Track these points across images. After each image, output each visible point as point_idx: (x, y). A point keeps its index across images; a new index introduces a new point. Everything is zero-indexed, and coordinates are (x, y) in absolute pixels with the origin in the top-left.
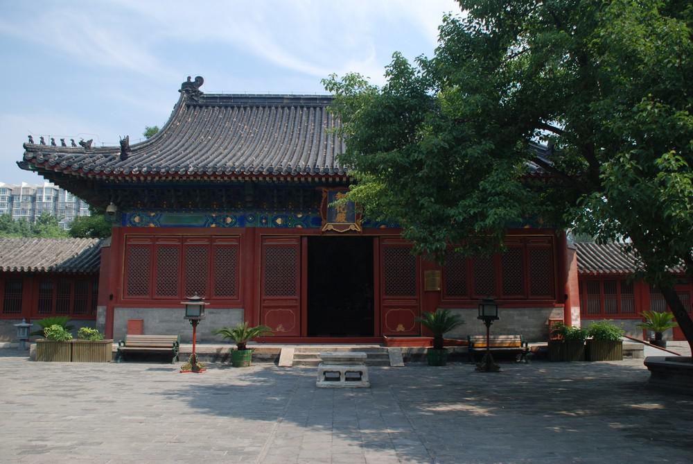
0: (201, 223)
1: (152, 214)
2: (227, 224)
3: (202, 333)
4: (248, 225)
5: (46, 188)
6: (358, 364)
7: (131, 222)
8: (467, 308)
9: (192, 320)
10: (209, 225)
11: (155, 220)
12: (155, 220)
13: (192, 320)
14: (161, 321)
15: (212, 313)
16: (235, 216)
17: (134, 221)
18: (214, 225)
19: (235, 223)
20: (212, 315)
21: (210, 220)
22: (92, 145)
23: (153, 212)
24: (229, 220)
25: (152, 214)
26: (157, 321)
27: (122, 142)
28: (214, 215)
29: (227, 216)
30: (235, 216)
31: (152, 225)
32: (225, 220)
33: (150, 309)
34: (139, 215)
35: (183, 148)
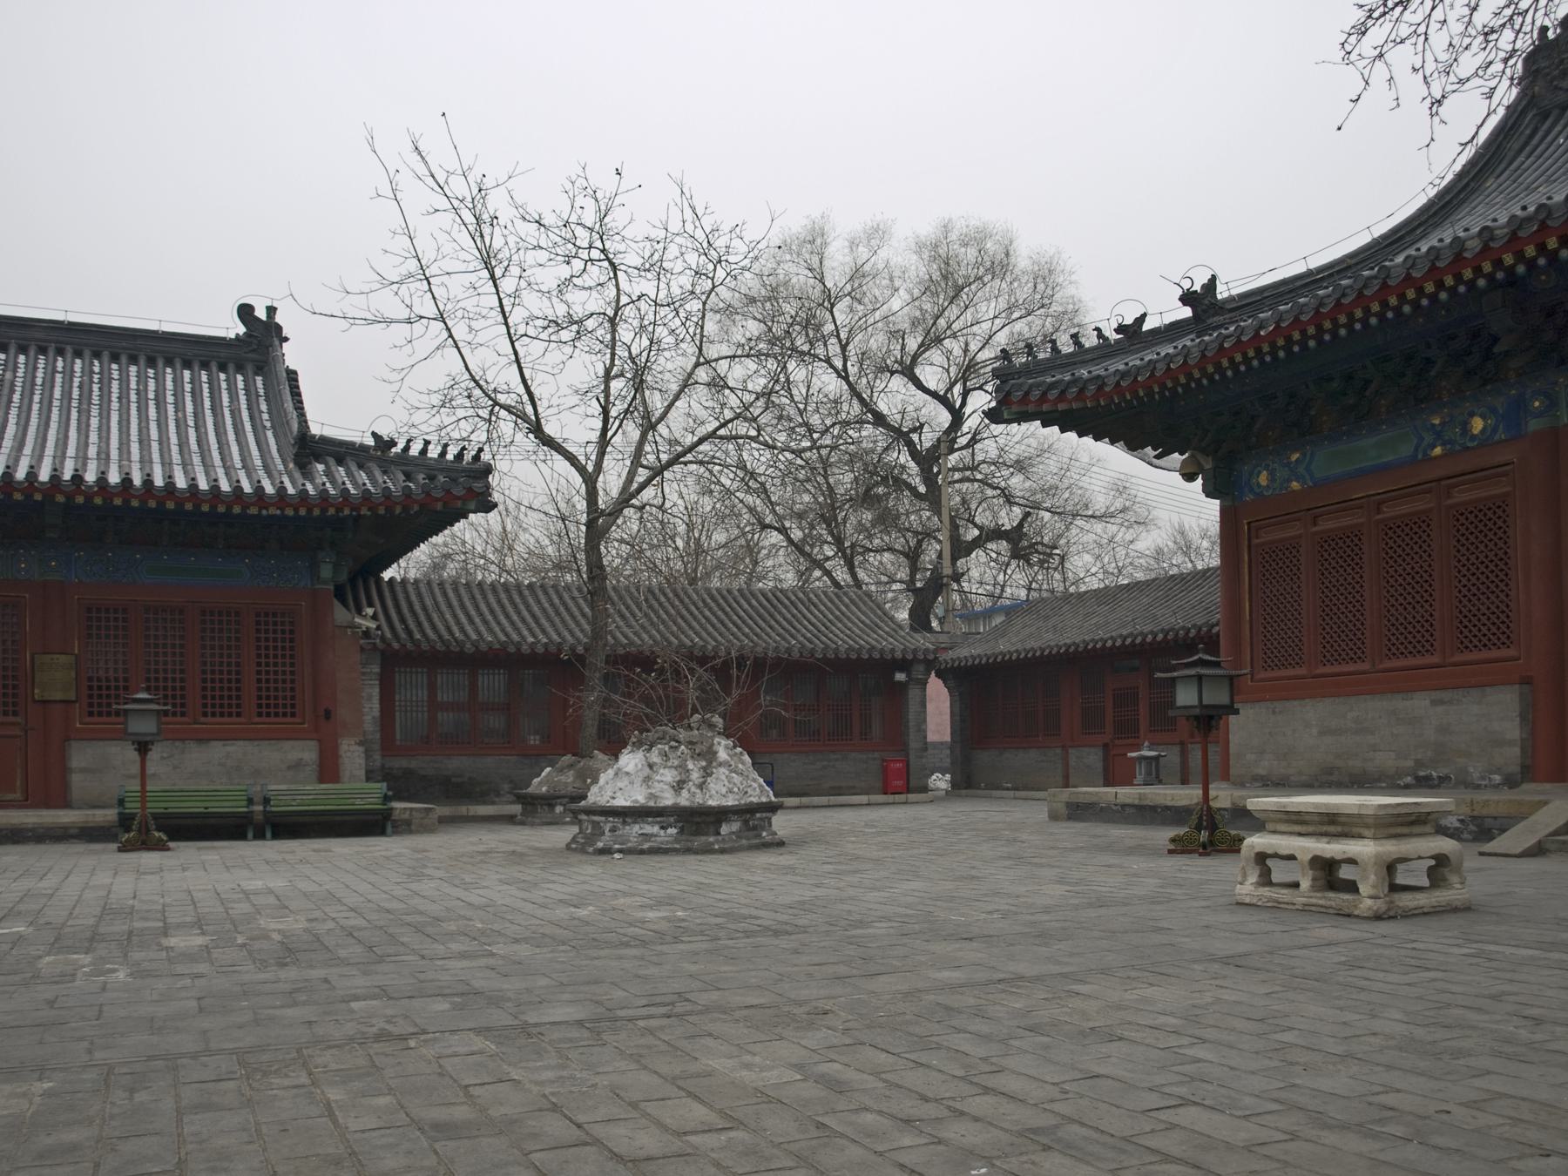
0: (1405, 450)
1: (1295, 456)
2: (1473, 437)
3: (1417, 761)
4: (1534, 425)
5: (613, 660)
6: (1361, 837)
7: (1251, 490)
8: (1372, 693)
9: (139, 743)
10: (1425, 454)
11: (1301, 470)
12: (1301, 470)
13: (139, 743)
14: (1322, 733)
15: (1441, 702)
16: (1493, 410)
17: (1483, 417)
18: (1438, 451)
19: (1495, 430)
20: (1440, 709)
21: (1428, 438)
22: (1222, 293)
23: (1296, 450)
24: (1478, 425)
25: (1295, 456)
26: (1315, 731)
27: (1187, 298)
28: (1437, 422)
29: (1472, 415)
30: (1493, 410)
31: (1295, 485)
32: (1465, 427)
33: (1296, 703)
34: (1267, 468)
35: (647, 624)
